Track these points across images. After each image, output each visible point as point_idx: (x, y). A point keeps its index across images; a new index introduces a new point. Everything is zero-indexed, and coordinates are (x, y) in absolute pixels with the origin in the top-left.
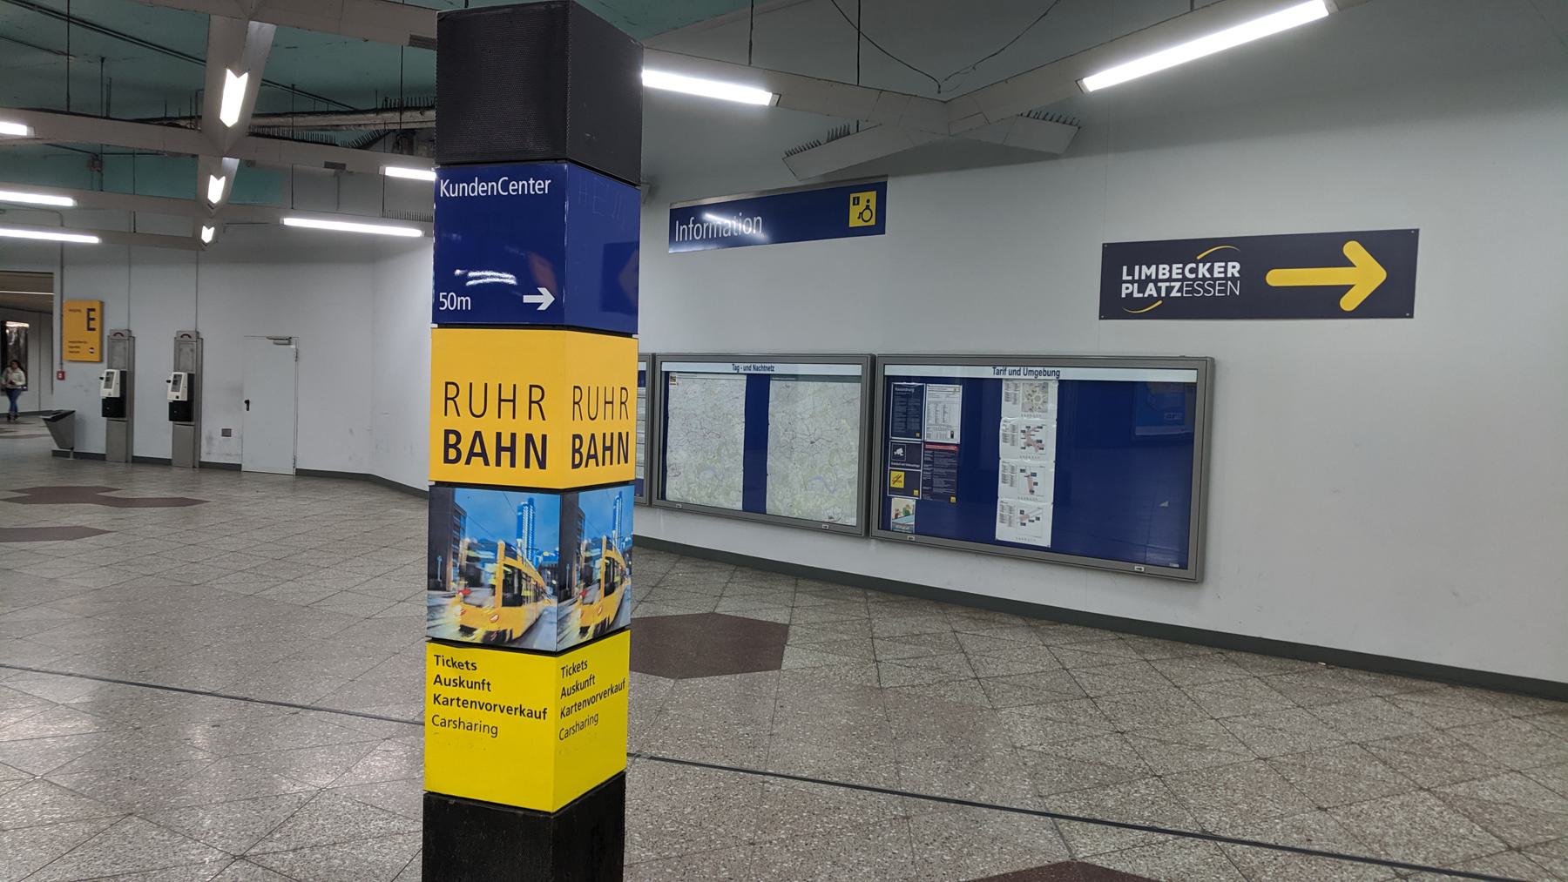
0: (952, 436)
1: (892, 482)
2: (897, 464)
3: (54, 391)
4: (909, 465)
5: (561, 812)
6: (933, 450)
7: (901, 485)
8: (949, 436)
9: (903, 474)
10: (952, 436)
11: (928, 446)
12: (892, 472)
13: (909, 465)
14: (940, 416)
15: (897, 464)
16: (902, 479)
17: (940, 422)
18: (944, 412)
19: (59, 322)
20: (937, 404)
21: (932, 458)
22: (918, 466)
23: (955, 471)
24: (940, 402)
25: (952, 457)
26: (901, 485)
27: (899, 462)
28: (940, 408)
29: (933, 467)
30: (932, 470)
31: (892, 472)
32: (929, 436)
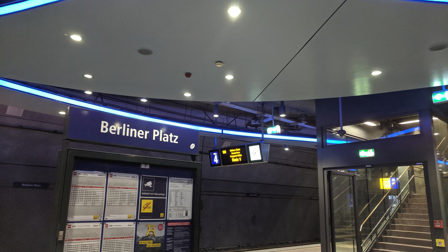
0: (187, 214)
1: (142, 209)
2: (147, 194)
3: (222, 61)
4: (157, 194)
5: (15, 82)
6: (174, 227)
7: (150, 210)
8: (184, 214)
9: (152, 201)
10: (187, 214)
11: (170, 224)
12: (143, 200)
13: (157, 194)
14: (178, 200)
15: (147, 194)
16: (151, 205)
17: (179, 205)
18: (182, 198)
19: (325, 188)
20: (176, 191)
21: (173, 233)
22: (163, 195)
23: (188, 240)
24: (179, 190)
25: (186, 230)
26: (150, 210)
27: (148, 192)
28: (179, 194)
29: (173, 239)
30: (173, 242)
31: (143, 200)
32: (170, 215)
